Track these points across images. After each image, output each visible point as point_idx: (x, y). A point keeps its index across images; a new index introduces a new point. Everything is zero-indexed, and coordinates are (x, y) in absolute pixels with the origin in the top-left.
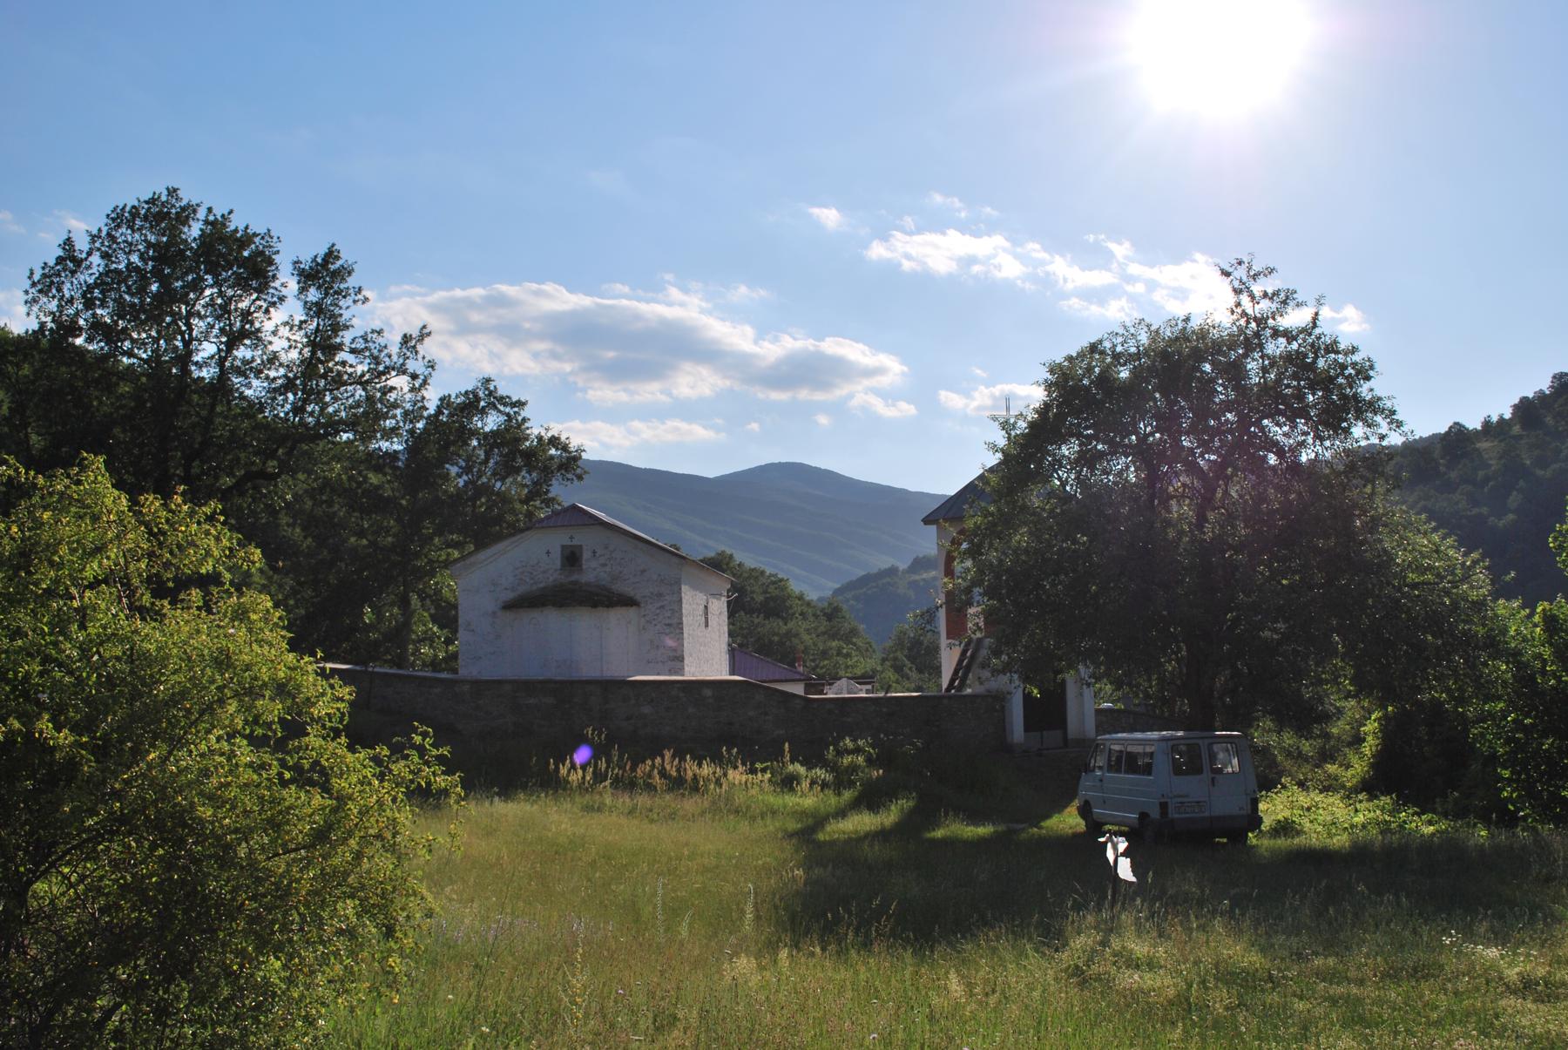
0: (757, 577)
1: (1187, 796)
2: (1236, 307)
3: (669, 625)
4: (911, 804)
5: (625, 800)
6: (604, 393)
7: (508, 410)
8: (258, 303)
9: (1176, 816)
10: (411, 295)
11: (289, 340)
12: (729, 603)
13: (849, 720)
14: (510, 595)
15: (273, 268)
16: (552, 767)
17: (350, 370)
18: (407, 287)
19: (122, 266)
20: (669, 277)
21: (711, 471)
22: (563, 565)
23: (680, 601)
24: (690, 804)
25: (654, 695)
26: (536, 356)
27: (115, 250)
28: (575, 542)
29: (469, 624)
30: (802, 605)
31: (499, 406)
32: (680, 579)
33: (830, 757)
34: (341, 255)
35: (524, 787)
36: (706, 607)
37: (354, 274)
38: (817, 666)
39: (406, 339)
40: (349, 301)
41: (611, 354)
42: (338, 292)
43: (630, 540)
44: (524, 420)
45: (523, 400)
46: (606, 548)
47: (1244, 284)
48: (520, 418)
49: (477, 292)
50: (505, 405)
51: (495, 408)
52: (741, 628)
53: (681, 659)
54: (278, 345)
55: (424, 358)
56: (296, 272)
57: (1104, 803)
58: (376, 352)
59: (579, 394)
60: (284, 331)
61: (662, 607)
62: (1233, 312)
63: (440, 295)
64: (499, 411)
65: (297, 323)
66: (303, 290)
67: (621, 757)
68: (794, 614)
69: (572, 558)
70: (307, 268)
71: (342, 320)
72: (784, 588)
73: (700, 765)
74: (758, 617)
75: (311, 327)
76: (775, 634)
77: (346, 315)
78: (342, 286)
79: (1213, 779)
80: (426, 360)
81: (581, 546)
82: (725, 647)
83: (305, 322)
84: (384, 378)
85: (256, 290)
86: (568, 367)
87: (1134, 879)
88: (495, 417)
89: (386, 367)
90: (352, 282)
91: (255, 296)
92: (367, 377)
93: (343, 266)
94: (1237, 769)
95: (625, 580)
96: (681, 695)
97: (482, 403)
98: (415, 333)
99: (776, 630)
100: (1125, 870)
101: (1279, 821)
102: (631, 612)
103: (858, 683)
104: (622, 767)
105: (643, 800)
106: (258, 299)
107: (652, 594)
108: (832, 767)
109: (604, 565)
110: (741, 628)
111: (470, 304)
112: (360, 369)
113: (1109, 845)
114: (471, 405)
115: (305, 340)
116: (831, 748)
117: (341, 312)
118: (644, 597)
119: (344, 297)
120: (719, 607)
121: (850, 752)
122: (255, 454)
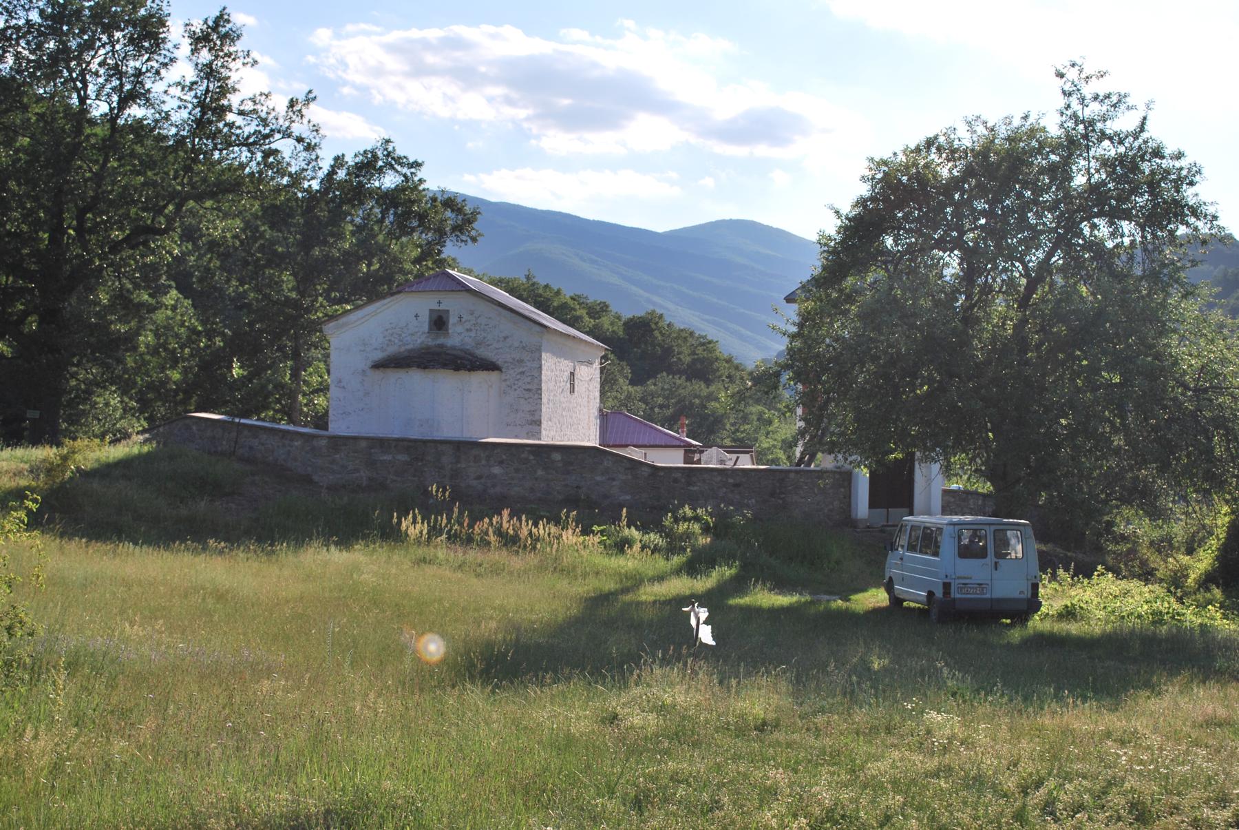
0: (685, 338)
1: (971, 578)
2: (1066, 109)
4: (733, 571)
5: (460, 554)
6: (557, 141)
7: (405, 170)
8: (150, 63)
9: (958, 596)
10: (368, 34)
11: (181, 99)
13: (695, 488)
14: (378, 356)
15: (165, 30)
17: (238, 131)
18: (363, 26)
19: (21, 22)
20: (630, 23)
21: (660, 226)
22: (430, 329)
23: (540, 367)
24: (516, 562)
25: (504, 457)
26: (491, 100)
27: (15, 6)
28: (442, 307)
29: (340, 382)
30: (729, 368)
31: (396, 166)
32: (540, 346)
33: (667, 523)
34: (231, 19)
35: (365, 537)
36: (572, 374)
37: (242, 38)
38: (737, 430)
39: (292, 103)
40: (239, 63)
41: (566, 102)
42: (229, 55)
43: (495, 307)
44: (421, 181)
45: (420, 161)
47: (1075, 86)
48: (416, 179)
49: (433, 34)
50: (401, 164)
51: (392, 167)
52: (663, 389)
53: (538, 423)
54: (170, 104)
55: (309, 122)
56: (187, 35)
57: (903, 580)
58: (263, 115)
59: (533, 142)
60: (176, 91)
61: (523, 373)
62: (1062, 114)
63: (395, 36)
64: (397, 171)
65: (188, 84)
66: (195, 51)
67: (461, 513)
68: (721, 376)
69: (439, 322)
70: (198, 31)
71: (230, 85)
72: (712, 351)
73: (536, 525)
74: (680, 378)
75: (201, 88)
76: (696, 396)
77: (234, 77)
78: (232, 49)
79: (996, 563)
80: (312, 124)
81: (448, 311)
82: (595, 412)
83: (196, 83)
84: (267, 141)
85: (147, 50)
86: (522, 113)
87: (713, 643)
88: (392, 177)
89: (272, 130)
90: (239, 46)
91: (146, 56)
92: (251, 140)
93: (231, 29)
94: (1020, 555)
95: (488, 345)
97: (380, 163)
98: (301, 97)
99: (698, 393)
100: (706, 635)
101: (1067, 607)
102: (493, 376)
103: (728, 452)
104: (461, 524)
105: (474, 555)
106: (149, 60)
107: (514, 359)
108: (669, 534)
109: (469, 330)
110: (663, 389)
111: (426, 45)
112: (248, 130)
113: (692, 614)
114: (368, 165)
115: (195, 101)
116: (670, 514)
117: (229, 74)
118: (505, 362)
119: (234, 59)
120: (590, 376)
121: (685, 519)
122: (144, 209)
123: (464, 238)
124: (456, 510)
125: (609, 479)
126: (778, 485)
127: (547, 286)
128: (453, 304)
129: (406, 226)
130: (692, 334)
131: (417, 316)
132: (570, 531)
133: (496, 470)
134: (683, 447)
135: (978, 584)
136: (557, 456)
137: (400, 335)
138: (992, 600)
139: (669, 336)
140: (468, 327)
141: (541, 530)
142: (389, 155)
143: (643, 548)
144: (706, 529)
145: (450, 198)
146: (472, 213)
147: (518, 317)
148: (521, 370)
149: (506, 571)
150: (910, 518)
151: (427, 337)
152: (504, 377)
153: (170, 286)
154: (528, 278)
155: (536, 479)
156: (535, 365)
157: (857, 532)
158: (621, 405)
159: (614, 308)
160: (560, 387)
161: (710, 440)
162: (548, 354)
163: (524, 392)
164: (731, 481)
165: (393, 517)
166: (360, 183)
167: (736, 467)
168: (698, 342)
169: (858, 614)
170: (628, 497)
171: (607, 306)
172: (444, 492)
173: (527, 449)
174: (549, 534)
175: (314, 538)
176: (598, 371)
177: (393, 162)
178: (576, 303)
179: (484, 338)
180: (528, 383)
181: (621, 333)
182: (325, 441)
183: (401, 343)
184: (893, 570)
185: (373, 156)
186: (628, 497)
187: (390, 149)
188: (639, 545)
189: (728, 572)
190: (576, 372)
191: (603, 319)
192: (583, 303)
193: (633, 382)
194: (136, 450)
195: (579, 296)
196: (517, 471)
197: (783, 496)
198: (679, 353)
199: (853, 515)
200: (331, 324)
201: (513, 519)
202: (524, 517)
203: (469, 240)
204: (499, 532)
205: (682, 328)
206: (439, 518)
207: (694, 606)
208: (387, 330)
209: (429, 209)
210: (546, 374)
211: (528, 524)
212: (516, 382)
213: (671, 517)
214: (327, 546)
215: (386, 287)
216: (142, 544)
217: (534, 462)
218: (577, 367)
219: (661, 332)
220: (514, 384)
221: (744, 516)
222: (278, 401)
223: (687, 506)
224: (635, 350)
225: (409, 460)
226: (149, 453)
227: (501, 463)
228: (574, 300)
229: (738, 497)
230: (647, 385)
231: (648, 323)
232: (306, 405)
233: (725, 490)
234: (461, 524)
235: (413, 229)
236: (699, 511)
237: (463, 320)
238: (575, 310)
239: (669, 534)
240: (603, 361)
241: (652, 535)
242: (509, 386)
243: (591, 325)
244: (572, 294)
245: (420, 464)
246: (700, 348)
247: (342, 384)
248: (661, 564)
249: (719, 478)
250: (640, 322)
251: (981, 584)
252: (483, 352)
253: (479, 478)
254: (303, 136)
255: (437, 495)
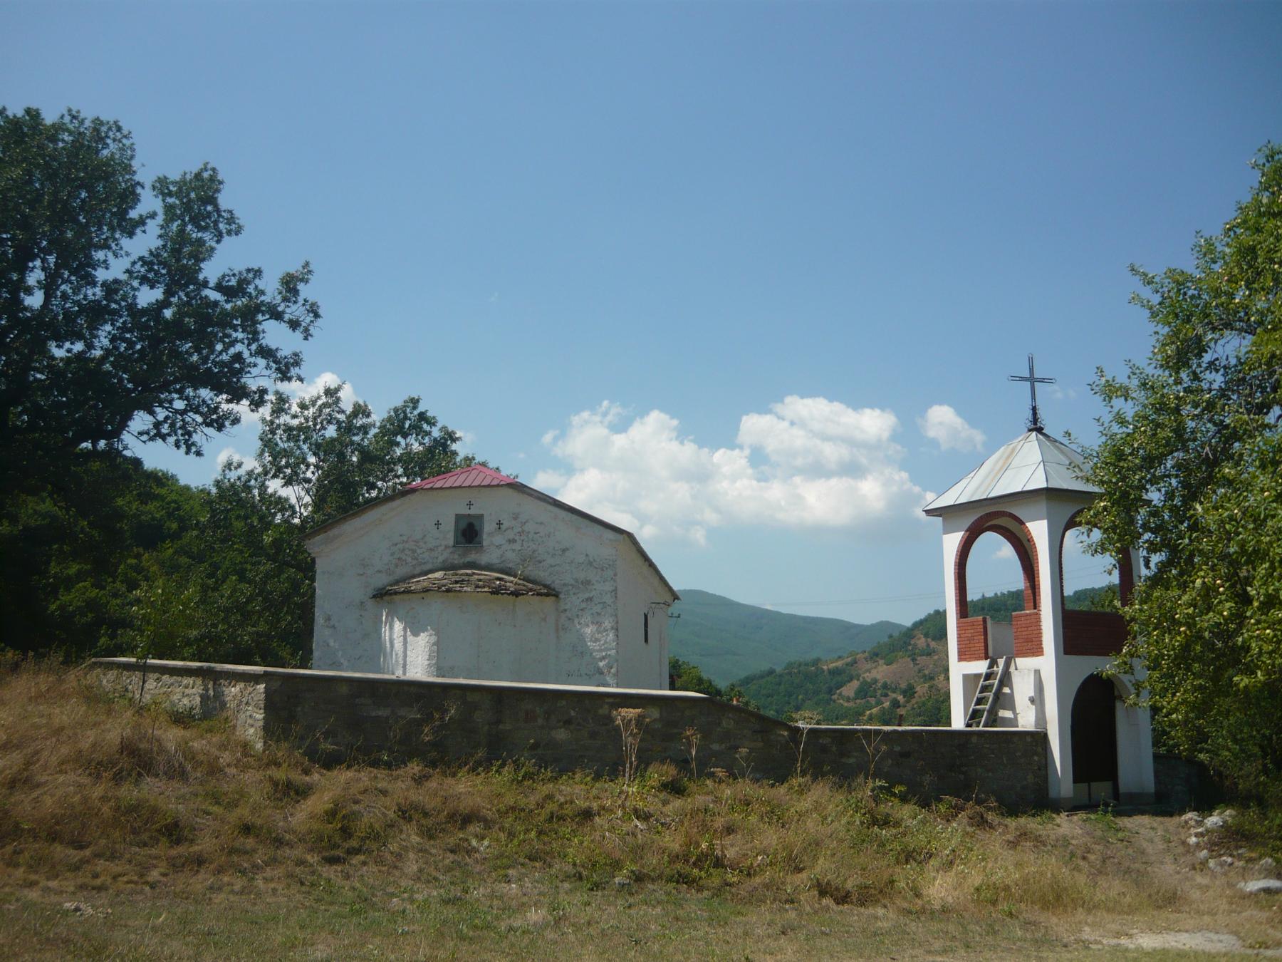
22: (457, 543)
25: (573, 713)
28: (473, 511)
61: (590, 599)
81: (482, 516)
107: (576, 580)
133: (561, 735)
137: (414, 551)
140: (511, 537)
148: (587, 595)
173: (607, 700)
179: (534, 551)
183: (415, 562)
197: (964, 769)
200: (318, 538)
208: (396, 545)
227: (568, 722)
237: (503, 527)
247: (332, 623)
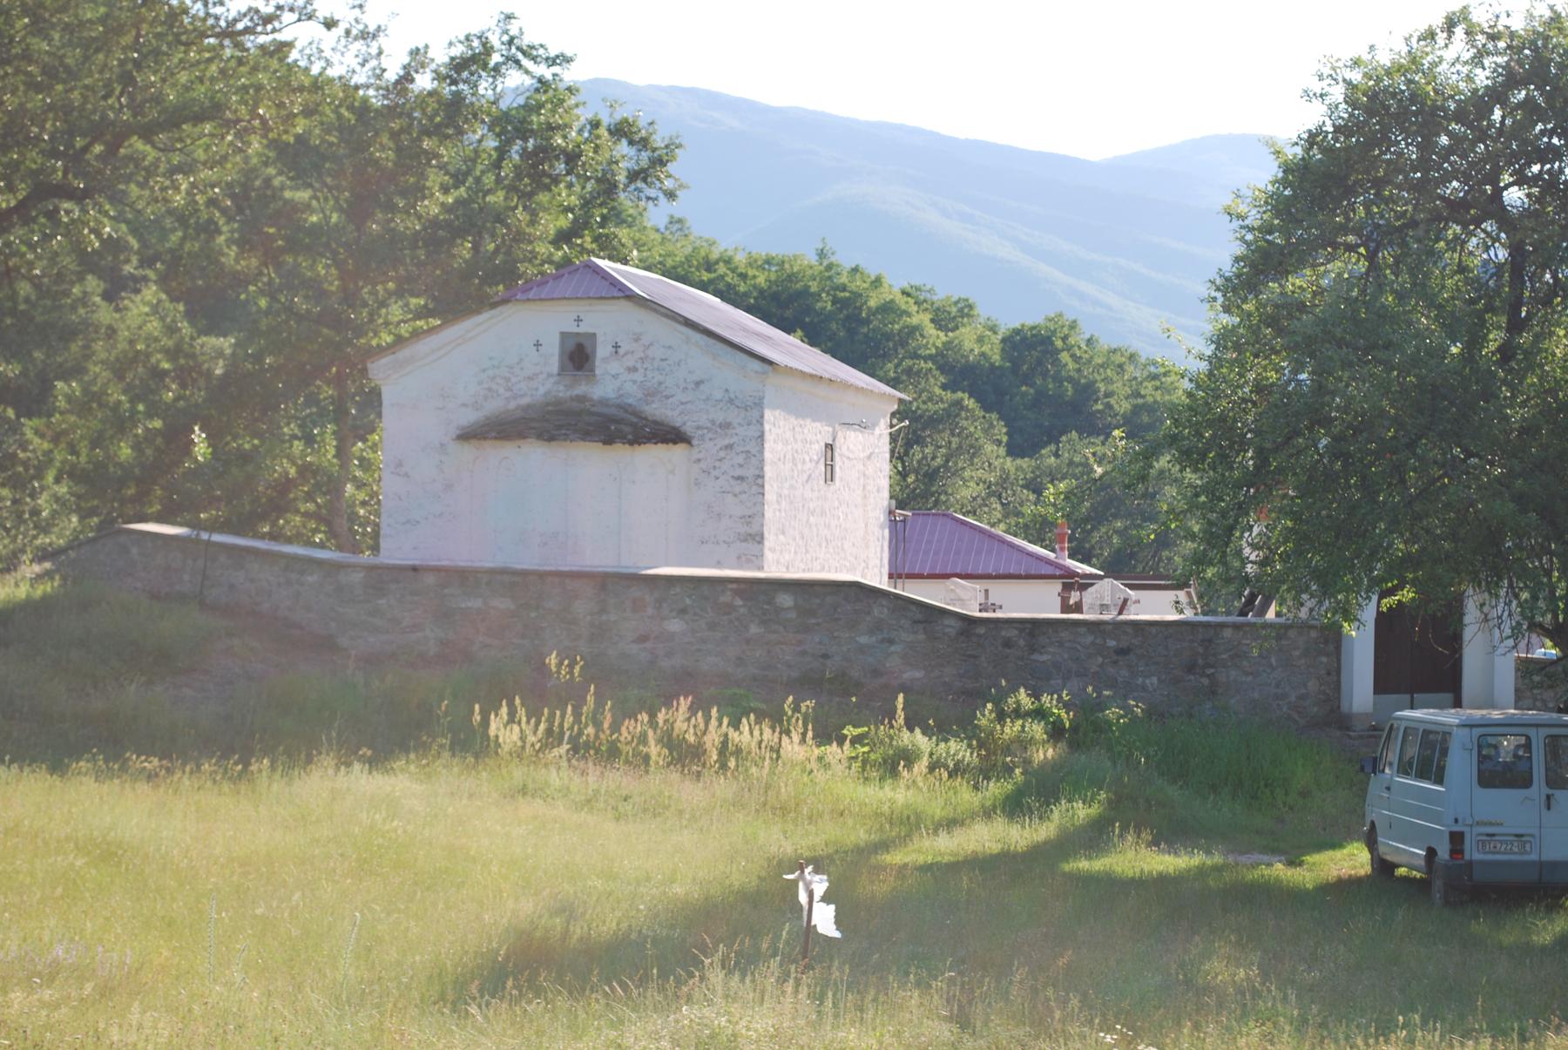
0: (1121, 366)
3: (741, 478)
4: (1094, 810)
9: (1477, 856)
12: (893, 438)
13: (1045, 658)
14: (469, 417)
16: (477, 717)
23: (761, 436)
24: (686, 791)
25: (688, 601)
28: (584, 328)
29: (400, 465)
32: (761, 399)
33: (984, 722)
36: (830, 447)
45: (569, 54)
46: (637, 340)
50: (534, 59)
53: (759, 538)
61: (730, 447)
64: (527, 72)
67: (600, 704)
69: (578, 356)
73: (736, 725)
79: (1548, 797)
81: (594, 334)
84: (269, 27)
87: (837, 935)
92: (240, 26)
95: (667, 397)
96: (739, 602)
97: (496, 58)
100: (824, 919)
102: (675, 454)
104: (598, 725)
105: (617, 779)
107: (713, 422)
108: (984, 743)
109: (633, 370)
113: (801, 885)
116: (989, 706)
118: (698, 428)
121: (1018, 713)
123: (652, 193)
124: (590, 699)
125: (882, 641)
126: (1201, 650)
127: (855, 270)
128: (603, 322)
129: (544, 173)
130: (1132, 357)
131: (538, 345)
132: (796, 737)
133: (675, 626)
134: (1060, 577)
135: (1517, 836)
136: (785, 600)
137: (508, 380)
138: (1541, 865)
139: (1090, 361)
140: (631, 364)
141: (746, 735)
142: (511, 42)
143: (932, 768)
144: (1056, 732)
145: (626, 120)
146: (667, 147)
147: (719, 345)
148: (726, 442)
149: (673, 808)
150: (1407, 713)
151: (557, 383)
152: (695, 454)
153: (145, 279)
154: (821, 254)
155: (748, 641)
156: (752, 431)
157: (1349, 736)
158: (989, 495)
159: (982, 311)
160: (803, 471)
161: (1160, 560)
162: (777, 412)
163: (733, 482)
164: (1112, 643)
165: (472, 712)
166: (457, 94)
167: (1122, 617)
168: (1145, 373)
169: (1307, 892)
170: (918, 674)
171: (971, 307)
172: (571, 666)
174: (760, 742)
175: (324, 751)
176: (887, 439)
177: (520, 56)
178: (911, 301)
180: (741, 466)
181: (996, 358)
182: (362, 575)
183: (508, 394)
184: (1378, 812)
185: (484, 45)
186: (918, 674)
187: (514, 31)
188: (925, 761)
189: (1082, 812)
190: (837, 445)
191: (963, 330)
192: (925, 301)
193: (1014, 451)
194: (22, 592)
195: (918, 289)
196: (712, 626)
198: (1108, 395)
199: (1345, 707)
201: (695, 714)
202: (714, 711)
203: (661, 196)
204: (671, 742)
205: (1114, 346)
206: (558, 713)
207: (803, 872)
208: (484, 371)
209: (586, 141)
210: (772, 449)
211: (720, 724)
212: (717, 464)
213: (991, 712)
214: (348, 765)
215: (501, 287)
216: (12, 762)
217: (742, 610)
218: (840, 434)
219: (1073, 356)
220: (715, 468)
221: (1128, 710)
222: (310, 497)
223: (1022, 690)
224: (1024, 388)
225: (512, 607)
226: (45, 597)
227: (683, 611)
228: (908, 295)
229: (1125, 672)
230: (1042, 456)
231: (1049, 338)
232: (364, 504)
233: (1100, 660)
234: (598, 725)
235: (556, 180)
236: (1045, 698)
237: (621, 351)
238: (909, 315)
239: (984, 743)
240: (895, 421)
241: (953, 745)
242: (706, 472)
243: (939, 344)
244: (905, 285)
245: (533, 615)
246: (1149, 385)
248: (966, 796)
249: (1090, 639)
250: (1033, 336)
251: (1522, 836)
252: (656, 410)
253: (643, 639)
254: (336, 18)
255: (559, 672)
